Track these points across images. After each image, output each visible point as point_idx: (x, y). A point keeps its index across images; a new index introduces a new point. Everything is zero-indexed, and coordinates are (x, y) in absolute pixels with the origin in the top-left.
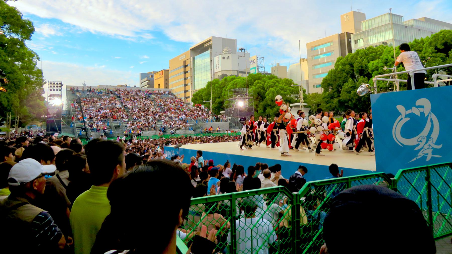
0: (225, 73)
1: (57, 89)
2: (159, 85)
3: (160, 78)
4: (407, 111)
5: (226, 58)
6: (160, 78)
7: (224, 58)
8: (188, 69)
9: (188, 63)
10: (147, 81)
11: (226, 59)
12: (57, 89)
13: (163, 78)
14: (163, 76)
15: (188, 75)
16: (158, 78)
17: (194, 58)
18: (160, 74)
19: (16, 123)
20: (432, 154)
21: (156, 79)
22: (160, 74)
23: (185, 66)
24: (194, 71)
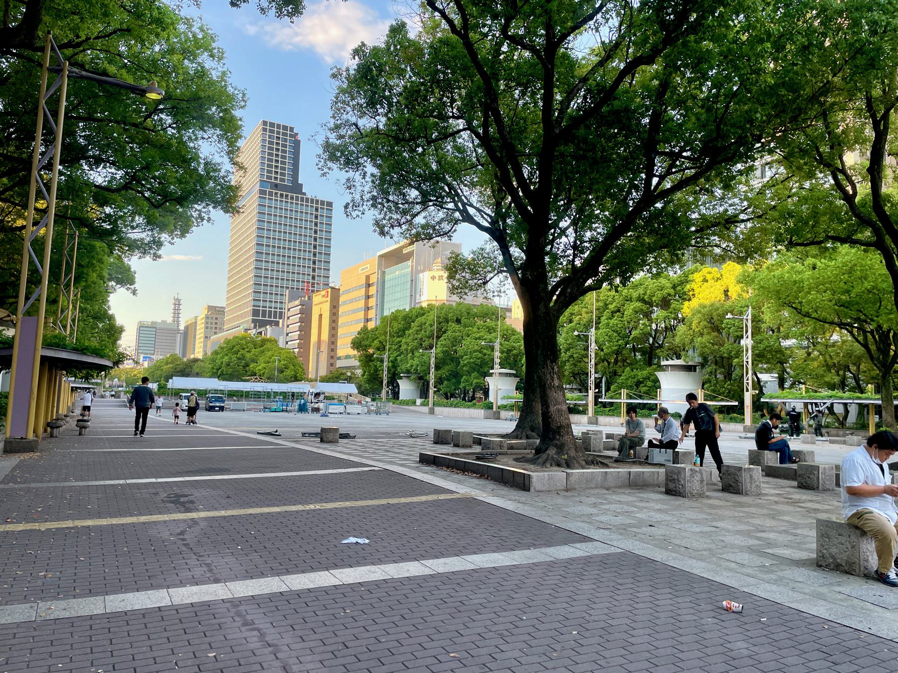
0: (430, 302)
1: (265, 304)
2: (321, 315)
3: (324, 302)
4: (841, 405)
5: (437, 278)
6: (324, 302)
7: (433, 278)
8: (373, 290)
9: (373, 279)
10: (300, 307)
11: (436, 280)
12: (265, 304)
13: (329, 303)
14: (329, 299)
15: (372, 302)
16: (321, 303)
17: (384, 273)
18: (323, 296)
19: (66, 275)
20: (142, 328)
21: (317, 304)
22: (323, 296)
23: (368, 285)
24: (383, 295)
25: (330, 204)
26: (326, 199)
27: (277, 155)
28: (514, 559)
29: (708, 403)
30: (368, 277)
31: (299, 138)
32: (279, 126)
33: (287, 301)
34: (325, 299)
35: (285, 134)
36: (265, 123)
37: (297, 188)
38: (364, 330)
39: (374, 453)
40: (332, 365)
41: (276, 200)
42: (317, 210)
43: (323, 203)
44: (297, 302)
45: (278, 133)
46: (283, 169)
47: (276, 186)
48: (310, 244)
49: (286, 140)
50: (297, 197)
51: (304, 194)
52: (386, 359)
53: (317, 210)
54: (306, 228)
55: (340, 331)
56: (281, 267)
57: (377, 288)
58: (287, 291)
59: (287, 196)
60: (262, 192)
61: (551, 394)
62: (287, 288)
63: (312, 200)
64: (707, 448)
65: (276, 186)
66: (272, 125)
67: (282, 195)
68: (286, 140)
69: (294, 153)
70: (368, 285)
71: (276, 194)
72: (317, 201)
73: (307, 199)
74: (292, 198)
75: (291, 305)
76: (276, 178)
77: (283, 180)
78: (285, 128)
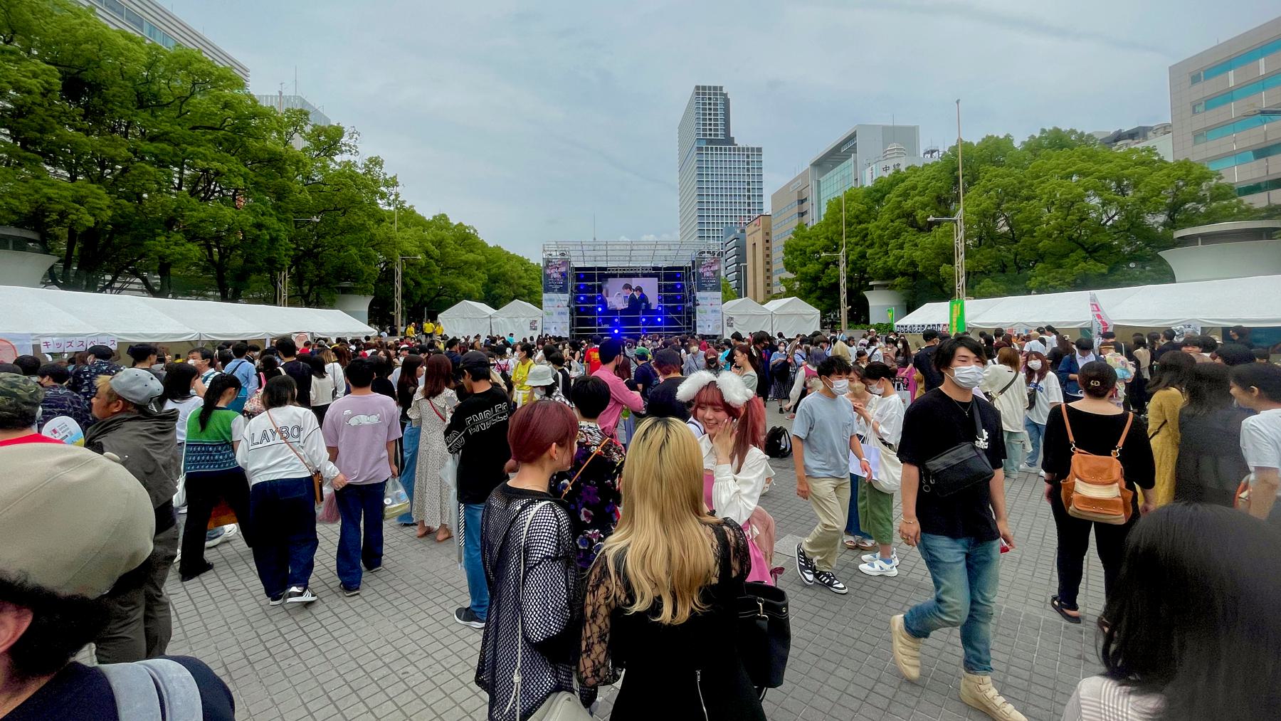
3: (756, 231)
6: (756, 231)
18: (756, 225)
26: (756, 146)
28: (968, 679)
29: (752, 596)
34: (757, 228)
35: (715, 94)
37: (729, 140)
38: (801, 227)
40: (769, 292)
42: (748, 157)
43: (753, 149)
45: (710, 94)
46: (716, 125)
47: (710, 142)
48: (744, 188)
50: (730, 148)
52: (842, 259)
53: (748, 157)
55: (774, 234)
59: (721, 148)
60: (700, 149)
61: (958, 546)
63: (743, 148)
64: (734, 574)
65: (710, 142)
66: (704, 88)
69: (724, 120)
72: (748, 149)
74: (725, 150)
76: (710, 135)
77: (717, 135)
78: (715, 88)
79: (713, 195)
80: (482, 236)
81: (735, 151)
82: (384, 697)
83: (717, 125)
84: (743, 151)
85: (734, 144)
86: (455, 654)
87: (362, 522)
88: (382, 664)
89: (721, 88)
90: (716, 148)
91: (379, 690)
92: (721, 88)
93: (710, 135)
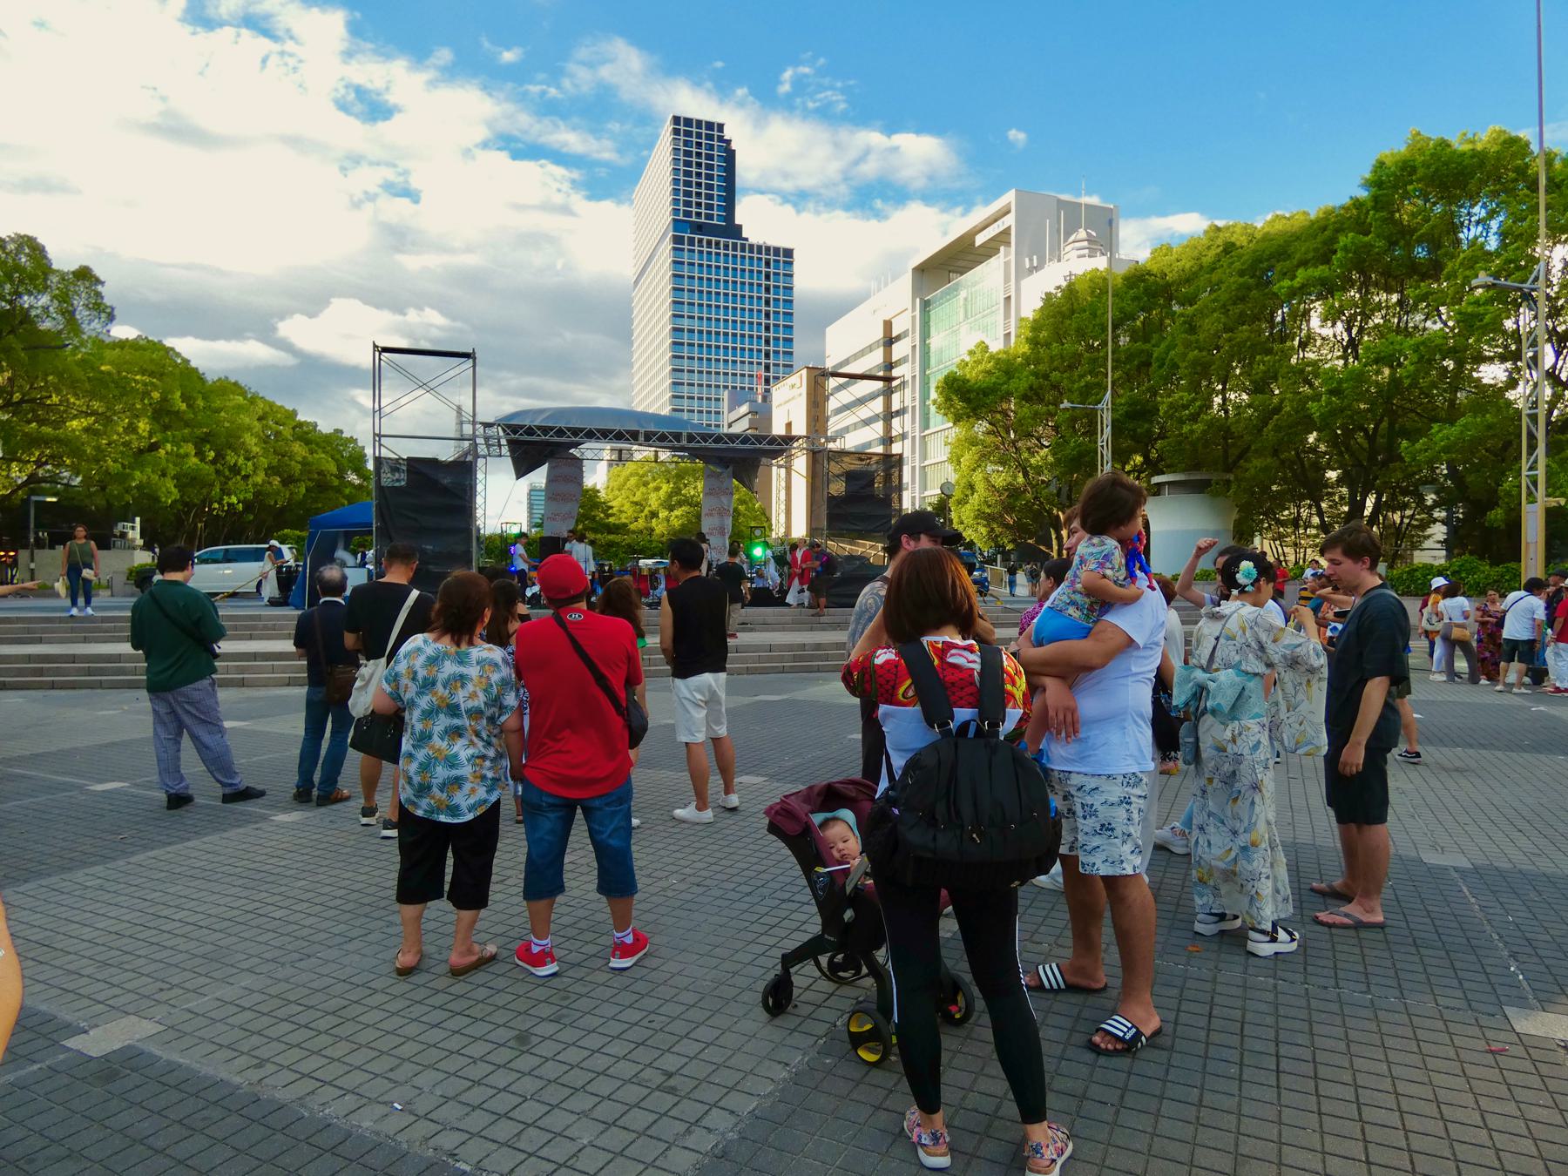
18: (793, 386)
23: (889, 341)
25: (789, 253)
27: (699, 175)
30: (888, 325)
31: (734, 146)
32: (699, 123)
33: (726, 410)
36: (676, 120)
37: (735, 231)
39: (101, 888)
41: (701, 252)
44: (744, 409)
45: (699, 135)
47: (699, 228)
49: (711, 147)
50: (735, 246)
51: (746, 239)
54: (710, 386)
56: (696, 391)
57: (913, 341)
58: (726, 392)
59: (717, 244)
60: (677, 240)
62: (726, 387)
63: (760, 247)
65: (699, 228)
66: (688, 122)
67: (709, 243)
68: (711, 147)
69: (725, 179)
70: (889, 341)
71: (700, 241)
72: (768, 249)
73: (751, 246)
75: (733, 416)
76: (699, 215)
78: (710, 125)
79: (701, 305)
80: (360, 303)
81: (743, 250)
82: (1272, 1050)
83: (710, 197)
84: (760, 252)
85: (740, 238)
86: (1418, 1040)
87: (448, 878)
88: (1286, 1111)
89: (721, 127)
90: (709, 243)
91: (1312, 1074)
92: (721, 127)
93: (699, 215)
